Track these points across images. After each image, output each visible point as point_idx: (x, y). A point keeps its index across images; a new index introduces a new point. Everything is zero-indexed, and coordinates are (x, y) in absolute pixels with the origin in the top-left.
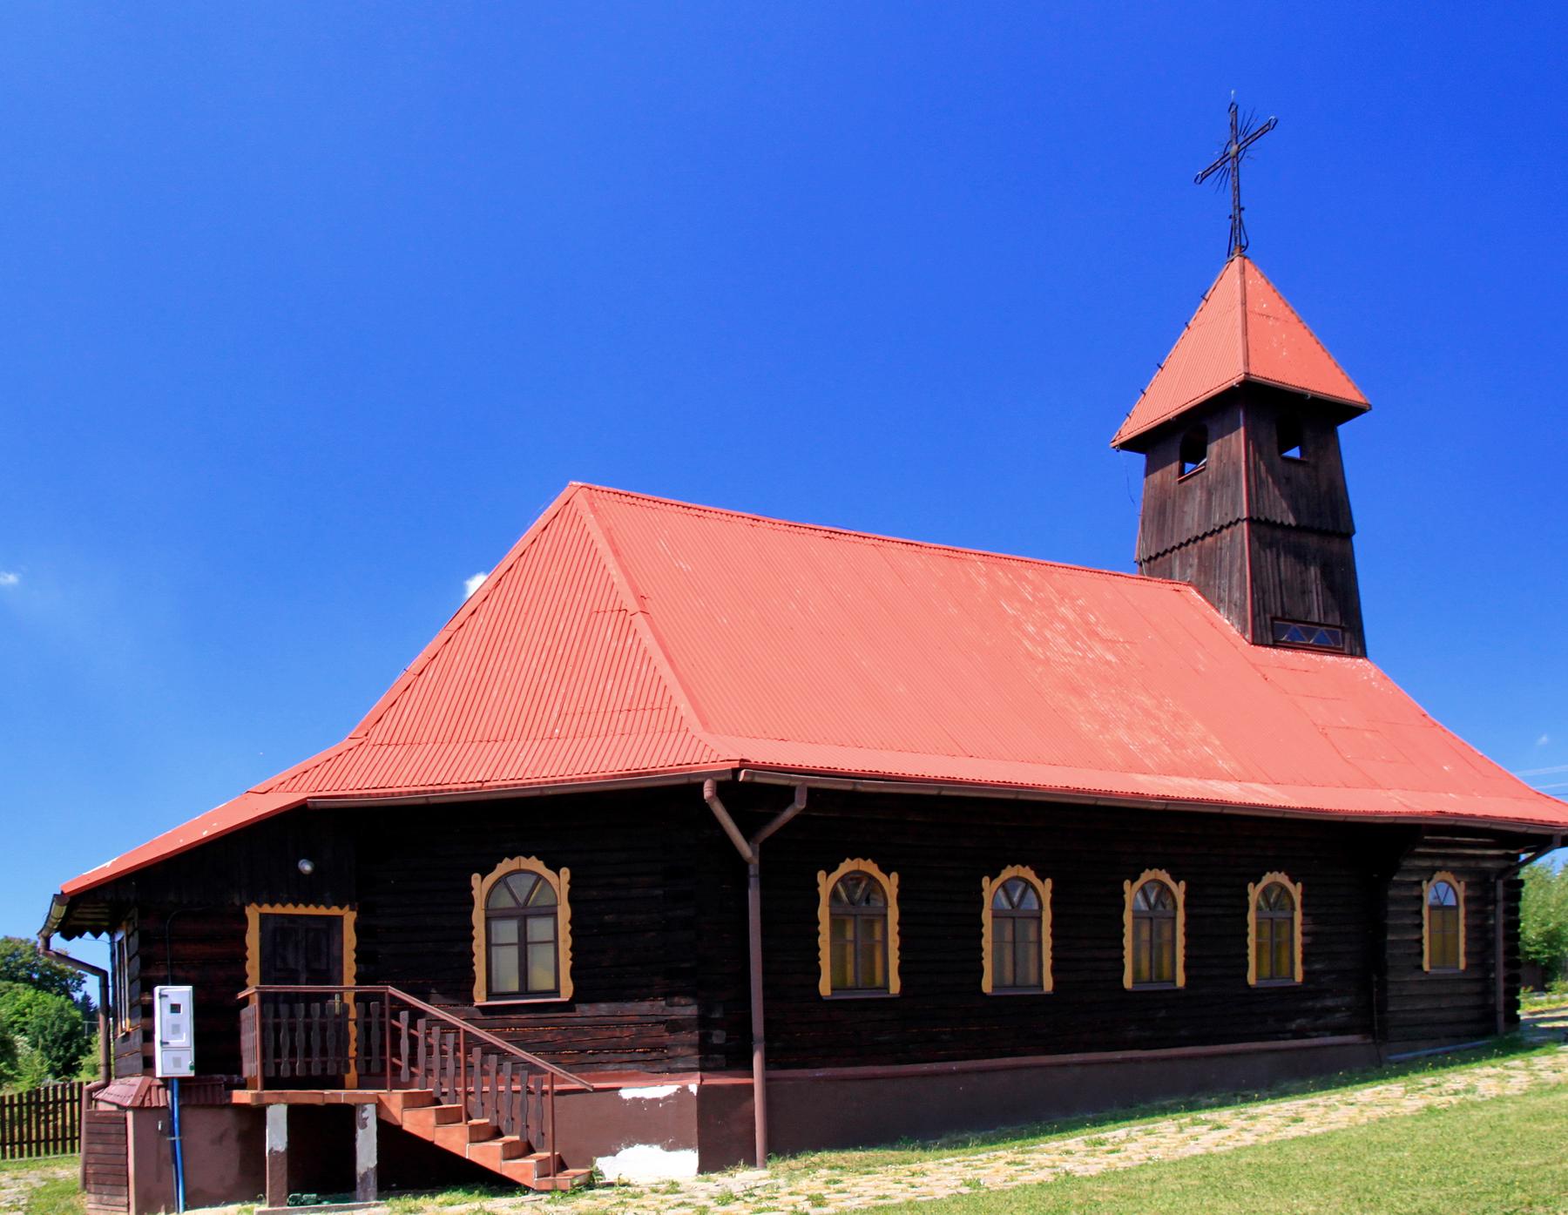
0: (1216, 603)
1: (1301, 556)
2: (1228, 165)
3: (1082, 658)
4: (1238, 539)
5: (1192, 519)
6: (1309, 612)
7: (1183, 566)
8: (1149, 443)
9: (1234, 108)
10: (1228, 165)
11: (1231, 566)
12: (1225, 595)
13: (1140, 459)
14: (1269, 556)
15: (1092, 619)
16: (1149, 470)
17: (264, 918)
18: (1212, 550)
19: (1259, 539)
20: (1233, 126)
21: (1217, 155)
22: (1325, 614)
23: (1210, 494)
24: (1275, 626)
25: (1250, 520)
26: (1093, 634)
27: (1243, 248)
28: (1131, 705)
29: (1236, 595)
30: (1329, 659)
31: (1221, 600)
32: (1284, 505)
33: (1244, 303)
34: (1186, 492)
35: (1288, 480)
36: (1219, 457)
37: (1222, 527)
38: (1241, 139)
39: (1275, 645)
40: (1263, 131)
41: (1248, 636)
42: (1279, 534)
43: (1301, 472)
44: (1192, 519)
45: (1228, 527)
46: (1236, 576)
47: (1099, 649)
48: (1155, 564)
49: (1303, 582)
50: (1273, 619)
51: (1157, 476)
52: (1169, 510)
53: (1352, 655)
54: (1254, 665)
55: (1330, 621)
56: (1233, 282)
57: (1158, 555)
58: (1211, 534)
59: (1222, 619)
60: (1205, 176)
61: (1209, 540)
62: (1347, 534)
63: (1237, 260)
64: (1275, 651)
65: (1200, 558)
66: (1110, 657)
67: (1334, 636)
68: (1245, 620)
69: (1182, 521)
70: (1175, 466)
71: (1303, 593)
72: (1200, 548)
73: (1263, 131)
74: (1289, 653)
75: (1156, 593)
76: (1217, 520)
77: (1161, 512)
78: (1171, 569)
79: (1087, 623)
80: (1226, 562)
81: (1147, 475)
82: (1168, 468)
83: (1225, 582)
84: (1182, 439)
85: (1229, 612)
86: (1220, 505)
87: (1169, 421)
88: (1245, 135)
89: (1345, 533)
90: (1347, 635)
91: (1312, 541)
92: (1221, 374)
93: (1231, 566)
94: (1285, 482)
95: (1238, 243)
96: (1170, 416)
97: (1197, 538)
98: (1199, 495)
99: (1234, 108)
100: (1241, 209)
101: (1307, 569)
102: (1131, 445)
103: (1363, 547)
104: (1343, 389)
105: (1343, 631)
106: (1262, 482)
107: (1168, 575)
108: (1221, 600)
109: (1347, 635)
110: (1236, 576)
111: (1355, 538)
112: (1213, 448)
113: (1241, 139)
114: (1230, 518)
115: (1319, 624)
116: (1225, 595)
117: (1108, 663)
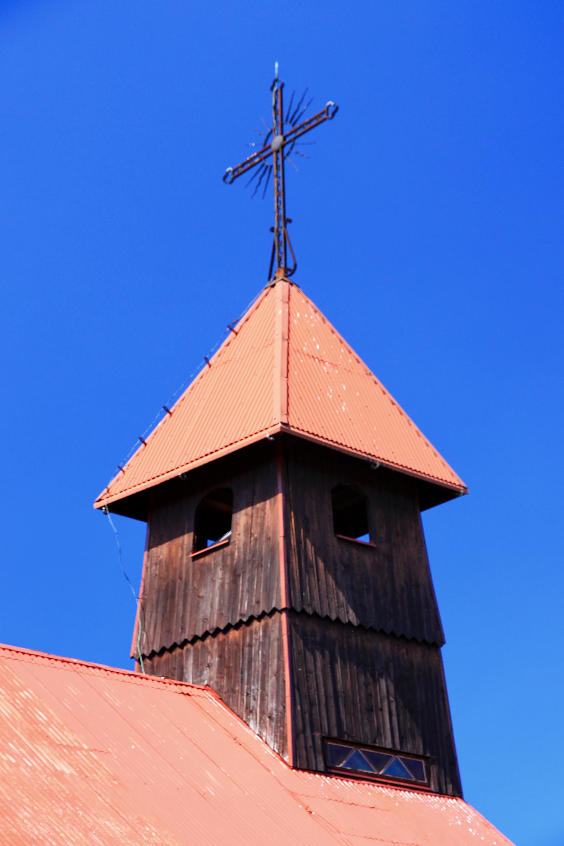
0: (244, 714)
1: (368, 666)
2: (265, 164)
3: (17, 765)
4: (275, 635)
5: (210, 606)
6: (379, 733)
7: (199, 667)
8: (154, 507)
9: (278, 86)
10: (271, 161)
11: (265, 666)
12: (256, 705)
13: (140, 528)
14: (318, 662)
15: (42, 716)
16: (154, 540)
17: (424, 780)
18: (239, 647)
19: (304, 635)
20: (278, 110)
21: (252, 150)
22: (401, 739)
23: (235, 576)
24: (325, 745)
25: (290, 611)
26: (38, 734)
27: (289, 273)
28: (86, 831)
29: (272, 705)
30: (407, 796)
31: (250, 711)
32: (342, 598)
33: (287, 339)
34: (203, 574)
35: (348, 568)
36: (248, 530)
37: (251, 619)
38: (288, 128)
39: (328, 772)
40: (319, 120)
41: (288, 758)
42: (333, 633)
43: (368, 559)
44: (210, 606)
45: (259, 618)
46: (271, 682)
47: (45, 754)
48: (162, 660)
49: (369, 696)
50: (323, 739)
51: (162, 551)
52: (179, 594)
53: (441, 793)
54: (293, 794)
55: (409, 748)
56: (278, 314)
57: (163, 650)
58: (237, 626)
59: (251, 732)
60: (237, 174)
61: (233, 634)
62: (435, 642)
63: (281, 286)
64: (328, 780)
65: (220, 656)
66: (61, 766)
67: (414, 767)
68: (283, 737)
69: (196, 607)
70: (188, 539)
71: (370, 710)
72: (222, 645)
73: (319, 120)
74: (349, 784)
75: (154, 694)
76: (245, 607)
77: (169, 596)
78: (182, 668)
79: (33, 721)
80: (258, 664)
81: (149, 548)
82: (179, 541)
83: (256, 687)
84: (196, 503)
85: (262, 724)
86: (250, 591)
87: (176, 479)
88: (296, 126)
89: (432, 640)
90: (434, 769)
91: (384, 647)
92: (259, 425)
93: (265, 666)
94: (344, 572)
95: (282, 263)
96: (178, 472)
97: (217, 631)
98: (220, 576)
99: (278, 86)
100: (287, 221)
101: (376, 681)
102: (125, 507)
103: (457, 663)
104: (433, 465)
105: (429, 760)
106: (309, 565)
107: (177, 675)
108: (250, 711)
109: (434, 769)
110: (271, 682)
111: (444, 650)
112: (241, 519)
113: (288, 128)
114: (262, 608)
115: (393, 751)
116: (256, 705)
117: (59, 775)
